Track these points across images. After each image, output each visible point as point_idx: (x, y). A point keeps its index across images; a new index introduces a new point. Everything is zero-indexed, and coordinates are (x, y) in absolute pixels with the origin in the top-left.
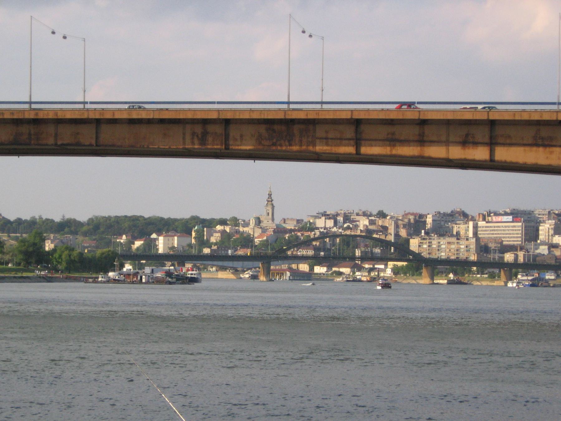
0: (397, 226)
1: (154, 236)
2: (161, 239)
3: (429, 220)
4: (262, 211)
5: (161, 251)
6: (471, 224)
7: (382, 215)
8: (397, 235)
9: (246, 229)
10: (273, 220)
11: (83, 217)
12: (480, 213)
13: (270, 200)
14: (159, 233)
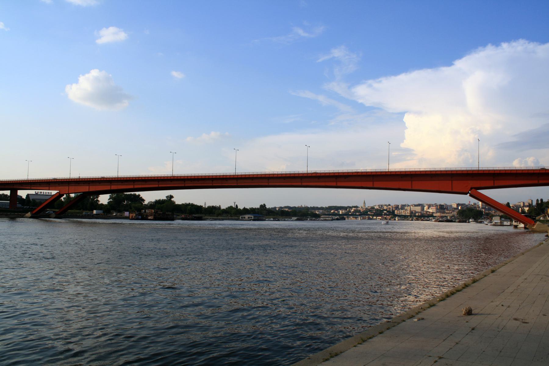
0: (393, 208)
1: (339, 210)
2: (340, 211)
3: (400, 206)
4: (362, 205)
6: (409, 207)
7: (389, 205)
8: (392, 210)
9: (359, 209)
10: (365, 206)
11: (324, 207)
12: (379, 204)
13: (364, 202)
14: (340, 210)
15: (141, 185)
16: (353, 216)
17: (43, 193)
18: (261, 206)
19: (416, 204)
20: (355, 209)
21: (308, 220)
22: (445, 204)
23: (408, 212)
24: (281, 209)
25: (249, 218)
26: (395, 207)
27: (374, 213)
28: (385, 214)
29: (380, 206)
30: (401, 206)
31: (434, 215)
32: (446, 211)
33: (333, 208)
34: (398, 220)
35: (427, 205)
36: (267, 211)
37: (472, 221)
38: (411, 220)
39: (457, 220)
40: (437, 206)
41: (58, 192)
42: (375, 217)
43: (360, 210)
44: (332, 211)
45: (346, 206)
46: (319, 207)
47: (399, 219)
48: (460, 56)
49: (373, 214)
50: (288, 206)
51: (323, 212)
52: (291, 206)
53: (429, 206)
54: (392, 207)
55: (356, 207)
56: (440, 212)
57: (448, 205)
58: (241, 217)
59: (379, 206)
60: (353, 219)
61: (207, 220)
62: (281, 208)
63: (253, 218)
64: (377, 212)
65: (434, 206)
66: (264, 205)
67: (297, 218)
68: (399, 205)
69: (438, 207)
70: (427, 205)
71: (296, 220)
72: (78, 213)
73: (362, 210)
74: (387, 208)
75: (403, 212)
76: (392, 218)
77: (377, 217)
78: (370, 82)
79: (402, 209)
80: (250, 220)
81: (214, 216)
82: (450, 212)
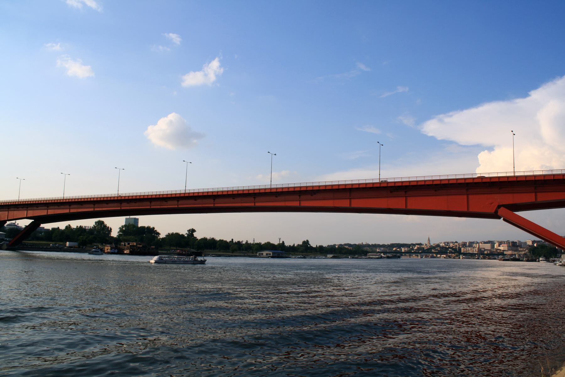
0: (459, 245)
1: (402, 248)
2: (403, 249)
3: (468, 243)
4: (427, 243)
5: (403, 251)
7: (456, 242)
8: (459, 247)
9: (423, 246)
11: (386, 244)
12: (445, 241)
15: (77, 208)
16: (415, 254)
17: (87, 227)
18: (304, 242)
19: (486, 240)
20: (418, 246)
21: (349, 257)
22: (518, 241)
23: (476, 250)
24: (340, 247)
25: (267, 254)
26: (462, 245)
27: (438, 251)
28: (451, 252)
29: (446, 243)
30: (469, 244)
31: (505, 253)
32: (520, 249)
33: (396, 245)
34: (463, 259)
35: (498, 242)
36: (258, 246)
37: (542, 260)
38: (477, 259)
39: (525, 259)
40: (509, 243)
41: (33, 221)
42: (439, 256)
43: (424, 248)
44: (394, 249)
45: (410, 243)
46: (381, 244)
47: (464, 257)
48: (535, 87)
49: (437, 251)
50: (348, 244)
51: (384, 250)
52: (352, 244)
53: (500, 243)
54: (459, 244)
55: (420, 244)
56: (512, 250)
57: (522, 242)
58: (258, 253)
59: (445, 243)
60: (415, 257)
61: (208, 256)
62: (341, 245)
63: (271, 255)
64: (442, 250)
65: (506, 243)
66: (308, 241)
67: (333, 255)
68: (466, 243)
69: (511, 244)
70: (498, 242)
71: (331, 258)
72: (45, 244)
73: (426, 248)
74: (453, 245)
75: (470, 250)
76: (457, 256)
77: (441, 255)
78: (441, 116)
79: (469, 247)
80: (268, 257)
81: (229, 252)
82: (524, 250)
